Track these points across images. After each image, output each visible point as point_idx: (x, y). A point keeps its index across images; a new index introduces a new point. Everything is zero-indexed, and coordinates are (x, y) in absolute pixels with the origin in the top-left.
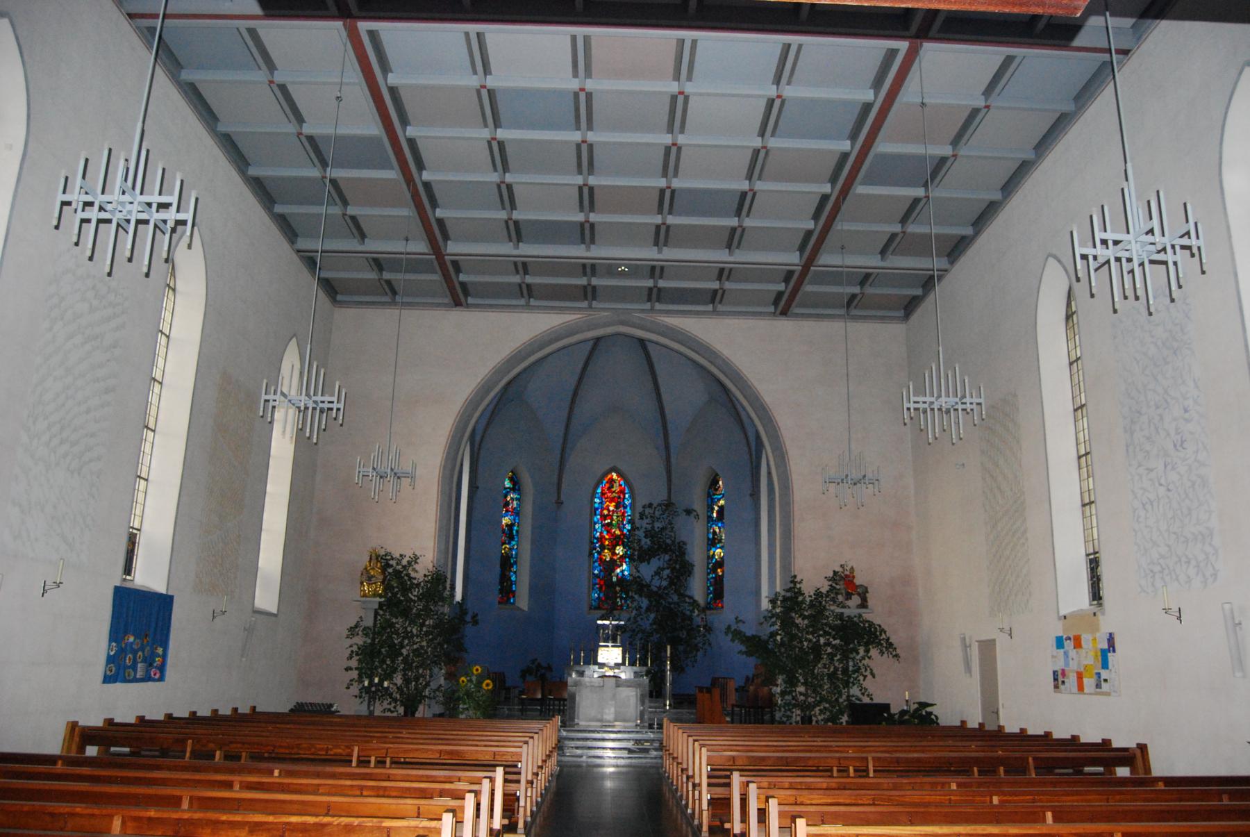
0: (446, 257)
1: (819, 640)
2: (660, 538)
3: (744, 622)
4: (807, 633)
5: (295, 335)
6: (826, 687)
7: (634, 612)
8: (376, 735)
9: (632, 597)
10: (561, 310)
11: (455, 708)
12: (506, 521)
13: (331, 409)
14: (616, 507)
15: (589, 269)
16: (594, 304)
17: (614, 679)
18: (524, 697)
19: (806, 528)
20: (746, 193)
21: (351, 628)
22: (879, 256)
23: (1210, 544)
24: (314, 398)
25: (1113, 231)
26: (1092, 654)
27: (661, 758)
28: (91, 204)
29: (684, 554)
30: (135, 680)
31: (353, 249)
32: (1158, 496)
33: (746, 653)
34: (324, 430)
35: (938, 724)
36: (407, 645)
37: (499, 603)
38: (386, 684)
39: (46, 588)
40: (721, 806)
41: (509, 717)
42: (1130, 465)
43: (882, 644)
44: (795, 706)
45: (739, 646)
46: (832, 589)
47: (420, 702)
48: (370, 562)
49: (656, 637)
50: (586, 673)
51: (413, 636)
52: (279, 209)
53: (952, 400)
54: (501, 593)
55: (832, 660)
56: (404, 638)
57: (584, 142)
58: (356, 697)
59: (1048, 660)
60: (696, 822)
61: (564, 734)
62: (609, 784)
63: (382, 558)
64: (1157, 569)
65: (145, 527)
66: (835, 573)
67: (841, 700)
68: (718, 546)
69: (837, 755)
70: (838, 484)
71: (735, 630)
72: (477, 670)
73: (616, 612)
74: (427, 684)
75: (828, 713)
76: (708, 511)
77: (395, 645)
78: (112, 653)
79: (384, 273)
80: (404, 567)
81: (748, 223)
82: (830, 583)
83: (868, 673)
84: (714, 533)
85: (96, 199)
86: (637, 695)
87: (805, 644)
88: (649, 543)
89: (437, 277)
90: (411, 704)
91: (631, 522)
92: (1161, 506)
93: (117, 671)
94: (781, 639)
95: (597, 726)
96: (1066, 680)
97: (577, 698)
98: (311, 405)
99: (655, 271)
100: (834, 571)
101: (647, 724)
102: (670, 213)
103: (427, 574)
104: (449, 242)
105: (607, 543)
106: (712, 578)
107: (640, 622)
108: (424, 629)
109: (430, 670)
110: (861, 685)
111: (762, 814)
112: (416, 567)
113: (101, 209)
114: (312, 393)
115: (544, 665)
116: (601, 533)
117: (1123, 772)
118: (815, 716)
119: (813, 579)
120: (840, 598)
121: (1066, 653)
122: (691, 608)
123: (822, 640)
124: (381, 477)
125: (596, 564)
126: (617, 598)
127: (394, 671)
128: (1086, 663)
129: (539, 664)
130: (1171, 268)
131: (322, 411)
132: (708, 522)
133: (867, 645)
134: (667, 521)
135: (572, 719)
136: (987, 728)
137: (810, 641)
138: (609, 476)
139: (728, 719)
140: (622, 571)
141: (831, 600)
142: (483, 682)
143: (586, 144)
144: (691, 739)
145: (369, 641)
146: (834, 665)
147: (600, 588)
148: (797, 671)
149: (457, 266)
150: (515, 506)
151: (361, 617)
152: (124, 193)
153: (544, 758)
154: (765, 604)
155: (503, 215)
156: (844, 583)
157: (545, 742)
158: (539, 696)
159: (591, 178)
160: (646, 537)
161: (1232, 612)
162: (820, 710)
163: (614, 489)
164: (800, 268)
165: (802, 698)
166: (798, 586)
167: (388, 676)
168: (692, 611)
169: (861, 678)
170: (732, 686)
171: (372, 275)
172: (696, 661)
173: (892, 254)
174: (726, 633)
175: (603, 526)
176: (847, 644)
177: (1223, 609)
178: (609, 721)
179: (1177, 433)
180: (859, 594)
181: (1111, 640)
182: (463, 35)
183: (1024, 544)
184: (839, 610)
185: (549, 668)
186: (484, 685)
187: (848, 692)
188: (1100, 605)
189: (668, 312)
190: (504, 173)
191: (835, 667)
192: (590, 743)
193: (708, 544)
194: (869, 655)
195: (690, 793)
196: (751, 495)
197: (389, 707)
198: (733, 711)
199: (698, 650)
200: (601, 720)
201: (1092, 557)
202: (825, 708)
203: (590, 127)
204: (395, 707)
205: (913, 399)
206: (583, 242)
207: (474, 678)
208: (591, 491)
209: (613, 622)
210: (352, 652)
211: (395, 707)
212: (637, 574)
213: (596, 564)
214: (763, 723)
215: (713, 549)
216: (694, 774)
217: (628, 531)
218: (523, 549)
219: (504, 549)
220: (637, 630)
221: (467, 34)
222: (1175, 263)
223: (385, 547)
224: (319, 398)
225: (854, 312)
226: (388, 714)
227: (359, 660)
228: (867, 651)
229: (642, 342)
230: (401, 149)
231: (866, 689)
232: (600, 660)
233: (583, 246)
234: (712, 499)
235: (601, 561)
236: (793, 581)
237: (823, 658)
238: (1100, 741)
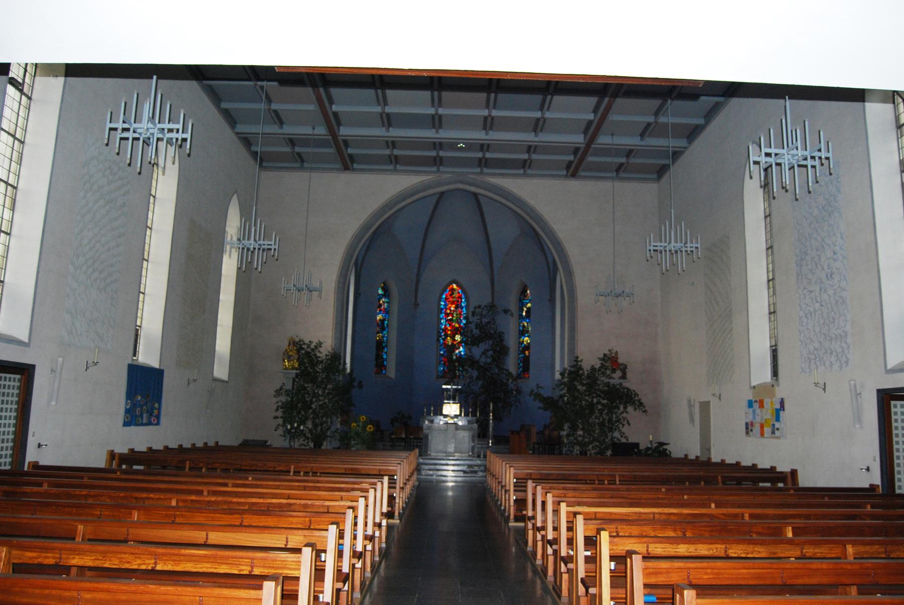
0: (339, 137)
1: (592, 401)
3: (542, 388)
4: (585, 396)
5: (235, 192)
6: (597, 431)
7: (468, 380)
8: (303, 459)
9: (466, 370)
10: (418, 173)
11: (348, 444)
12: (379, 317)
13: (271, 249)
14: (455, 308)
15: (438, 145)
16: (441, 168)
18: (393, 436)
19: (584, 324)
21: (277, 390)
22: (639, 138)
23: (845, 342)
24: (259, 242)
25: (775, 148)
26: (770, 412)
27: (485, 476)
28: (128, 130)
30: (142, 424)
31: (276, 132)
32: (815, 309)
33: (543, 408)
34: (265, 263)
35: (670, 456)
36: (315, 402)
37: (375, 373)
38: (302, 428)
39: (88, 365)
40: (521, 503)
41: (384, 449)
42: (799, 288)
43: (635, 404)
44: (575, 444)
45: (538, 404)
46: (602, 366)
47: (324, 440)
48: (289, 346)
51: (319, 395)
52: (224, 105)
53: (679, 245)
54: (376, 367)
55: (602, 413)
56: (313, 397)
59: (742, 415)
60: (507, 514)
61: (421, 461)
62: (450, 493)
64: (812, 357)
65: (144, 325)
66: (605, 355)
67: (607, 440)
68: (526, 335)
69: (597, 473)
70: (606, 296)
71: (536, 393)
72: (363, 418)
74: (329, 428)
75: (598, 449)
77: (307, 401)
78: (128, 407)
79: (296, 147)
80: (312, 350)
81: (548, 115)
82: (601, 362)
83: (625, 423)
84: (524, 326)
86: (469, 435)
87: (584, 402)
88: (478, 332)
89: (332, 150)
90: (318, 441)
91: (466, 318)
92: (817, 315)
93: (132, 418)
94: (568, 399)
95: (443, 456)
96: (753, 429)
97: (430, 437)
99: (484, 147)
101: (476, 455)
102: (494, 108)
103: (328, 354)
105: (449, 332)
106: (522, 357)
107: (473, 387)
108: (327, 391)
109: (331, 418)
110: (620, 431)
111: (544, 503)
112: (320, 349)
113: (134, 132)
114: (257, 239)
116: (445, 326)
117: (781, 485)
119: (589, 359)
120: (608, 372)
121: (754, 411)
122: (507, 378)
123: (595, 400)
124: (299, 291)
125: (442, 347)
126: (456, 370)
127: (307, 419)
128: (766, 417)
131: (264, 250)
132: (520, 319)
135: (426, 451)
136: (701, 459)
137: (587, 400)
138: (451, 287)
139: (530, 452)
140: (460, 352)
144: (504, 463)
145: (289, 399)
146: (603, 417)
147: (444, 364)
148: (577, 421)
149: (346, 143)
150: (386, 307)
151: (283, 383)
153: (405, 482)
154: (558, 376)
155: (379, 109)
156: (611, 362)
157: (410, 464)
158: (404, 436)
161: (855, 385)
162: (593, 447)
164: (584, 145)
165: (580, 438)
166: (580, 363)
167: (302, 422)
168: (508, 380)
169: (621, 426)
170: (534, 431)
171: (287, 149)
173: (648, 136)
175: (447, 321)
177: (850, 385)
179: (828, 269)
180: (621, 370)
181: (782, 403)
183: (730, 338)
184: (607, 380)
185: (410, 417)
186: (368, 429)
187: (612, 435)
188: (777, 380)
191: (603, 418)
192: (438, 467)
194: (627, 410)
195: (503, 496)
196: (549, 300)
197: (303, 442)
198: (534, 447)
199: (512, 406)
200: (445, 452)
201: (774, 348)
202: (596, 446)
205: (653, 244)
206: (434, 127)
207: (361, 424)
208: (438, 296)
209: (454, 387)
210: (278, 406)
211: (308, 443)
212: (470, 354)
214: (554, 454)
215: (523, 338)
216: (506, 484)
217: (464, 324)
218: (392, 337)
224: (262, 242)
225: (622, 175)
226: (304, 447)
227: (283, 412)
228: (625, 408)
229: (475, 195)
230: (330, 121)
231: (624, 433)
232: (445, 412)
233: (434, 130)
234: (523, 303)
235: (446, 345)
236: (576, 359)
237: (595, 412)
238: (769, 467)
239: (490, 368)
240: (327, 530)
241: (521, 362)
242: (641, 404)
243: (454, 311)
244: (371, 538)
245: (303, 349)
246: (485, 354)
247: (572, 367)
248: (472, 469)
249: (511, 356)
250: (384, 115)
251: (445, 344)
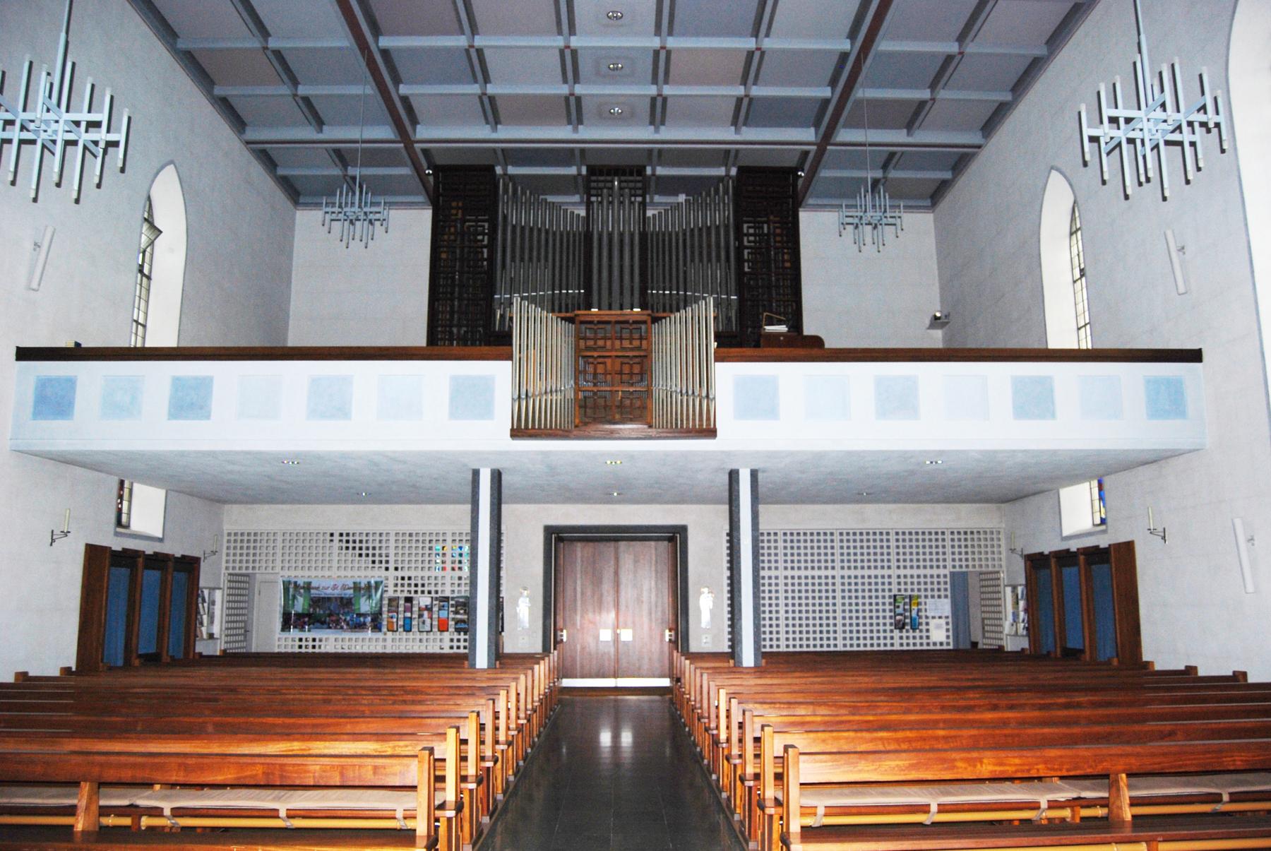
20: (753, 52)
25: (1125, 108)
85: (17, 117)
104: (419, 127)
113: (23, 128)
130: (1188, 149)
152: (48, 110)
159: (573, 39)
164: (814, 147)
203: (576, 79)
206: (569, 122)
222: (1193, 144)
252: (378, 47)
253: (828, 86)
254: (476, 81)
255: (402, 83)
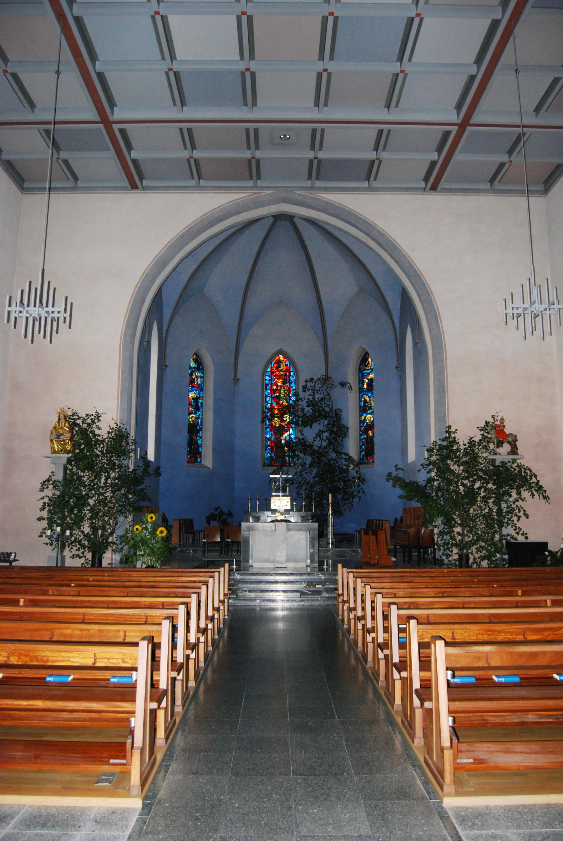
2: (320, 406)
7: (300, 467)
9: (298, 456)
10: (229, 189)
12: (192, 395)
16: (259, 183)
17: (284, 524)
24: (46, 309)
29: (340, 419)
37: (188, 462)
44: (453, 545)
46: (484, 437)
47: (106, 548)
49: (318, 488)
50: (262, 518)
54: (190, 454)
56: (90, 490)
57: (253, 158)
58: (47, 544)
63: (70, 418)
66: (487, 423)
68: (369, 412)
71: (396, 477)
72: (151, 518)
73: (285, 468)
76: (359, 384)
80: (89, 425)
82: (482, 432)
83: (521, 514)
84: (365, 401)
88: (311, 411)
98: (43, 315)
100: (486, 421)
102: (317, 178)
103: (111, 431)
106: (364, 438)
107: (305, 476)
115: (226, 511)
116: (271, 404)
118: (472, 553)
125: (268, 430)
127: (82, 519)
129: (221, 511)
132: (360, 393)
133: (518, 488)
134: (325, 393)
138: (277, 358)
141: (483, 448)
142: (157, 530)
143: (249, 73)
147: (272, 450)
155: (185, 154)
159: (257, 152)
160: (308, 406)
163: (281, 369)
166: (453, 435)
168: (348, 466)
169: (515, 518)
172: (352, 506)
174: (388, 480)
175: (272, 398)
176: (499, 487)
178: (282, 563)
180: (509, 443)
182: (178, 131)
184: (491, 457)
185: (230, 514)
186: (158, 532)
189: (326, 189)
190: (192, 150)
192: (263, 586)
193: (360, 411)
197: (77, 553)
199: (354, 497)
200: (274, 561)
203: (257, 148)
204: (83, 553)
206: (246, 104)
207: (149, 526)
208: (261, 370)
210: (44, 503)
211: (83, 553)
212: (302, 437)
213: (268, 430)
215: (364, 415)
217: (294, 402)
219: (191, 418)
220: (302, 482)
221: (181, 130)
223: (72, 408)
228: (519, 493)
232: (273, 507)
235: (272, 427)
239: (326, 452)
240: (177, 609)
241: (363, 445)
242: (540, 488)
243: (281, 386)
244: (204, 631)
245: (78, 425)
246: (320, 435)
247: (443, 440)
248: (312, 589)
249: (350, 436)
250: (192, 161)
251: (271, 425)
252: (131, 159)
253: (436, 151)
254: (193, 178)
255: (145, 179)
